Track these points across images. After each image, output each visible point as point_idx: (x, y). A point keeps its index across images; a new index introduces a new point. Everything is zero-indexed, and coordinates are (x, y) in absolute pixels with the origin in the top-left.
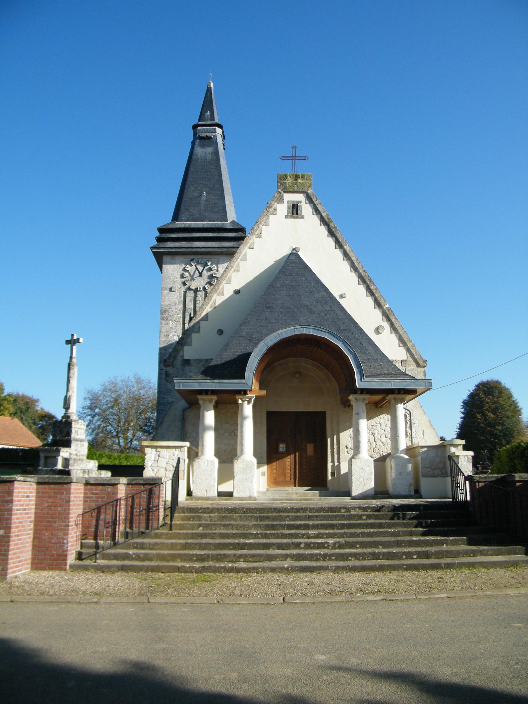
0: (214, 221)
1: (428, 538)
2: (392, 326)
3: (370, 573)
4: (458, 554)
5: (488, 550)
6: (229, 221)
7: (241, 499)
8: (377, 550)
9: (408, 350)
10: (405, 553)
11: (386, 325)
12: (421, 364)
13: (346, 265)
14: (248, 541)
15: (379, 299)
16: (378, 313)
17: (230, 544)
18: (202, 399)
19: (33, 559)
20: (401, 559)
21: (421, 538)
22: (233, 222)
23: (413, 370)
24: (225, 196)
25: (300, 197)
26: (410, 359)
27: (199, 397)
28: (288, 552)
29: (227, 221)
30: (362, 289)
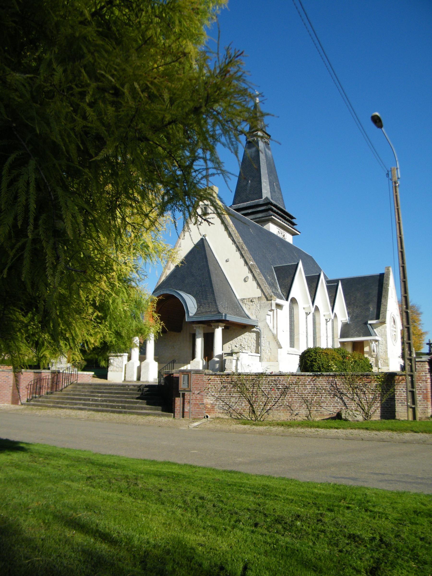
0: (254, 200)
1: (138, 400)
2: (254, 276)
3: (41, 409)
4: (142, 408)
5: (147, 407)
6: (263, 198)
7: (143, 382)
8: (114, 404)
9: (262, 290)
10: (117, 406)
11: (250, 276)
12: (269, 299)
13: (230, 241)
14: (127, 400)
15: (246, 259)
16: (246, 268)
17: (70, 398)
18: (214, 325)
19: (12, 400)
20: (115, 408)
21: (136, 400)
22: (267, 198)
23: (264, 303)
24: (262, 178)
25: (206, 202)
26: (263, 296)
27: (194, 325)
28: (81, 402)
29: (262, 198)
30: (238, 254)
